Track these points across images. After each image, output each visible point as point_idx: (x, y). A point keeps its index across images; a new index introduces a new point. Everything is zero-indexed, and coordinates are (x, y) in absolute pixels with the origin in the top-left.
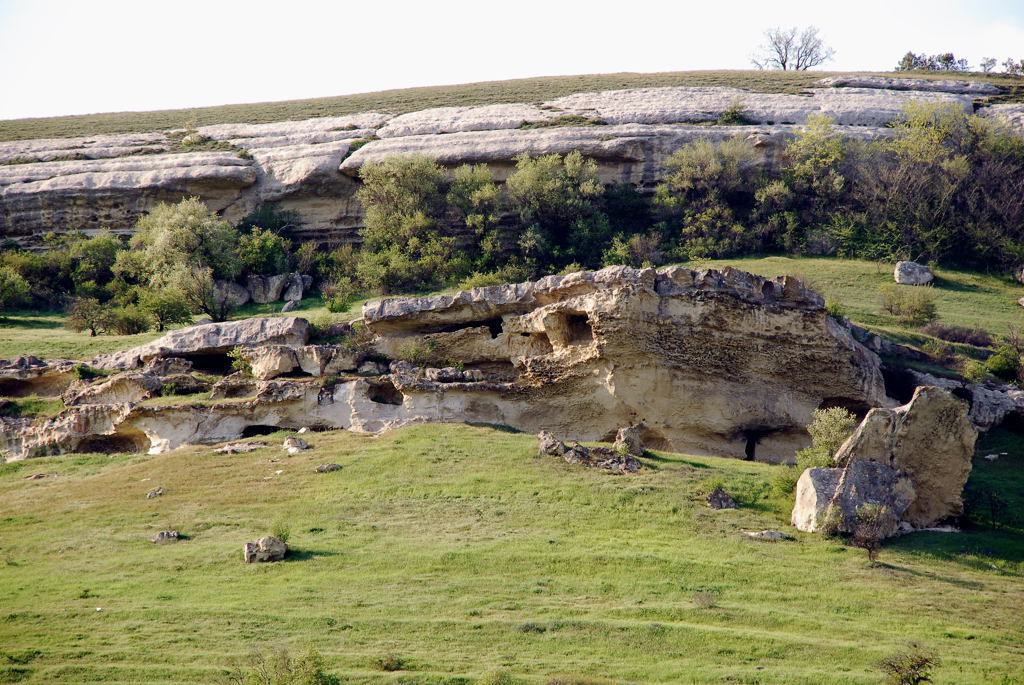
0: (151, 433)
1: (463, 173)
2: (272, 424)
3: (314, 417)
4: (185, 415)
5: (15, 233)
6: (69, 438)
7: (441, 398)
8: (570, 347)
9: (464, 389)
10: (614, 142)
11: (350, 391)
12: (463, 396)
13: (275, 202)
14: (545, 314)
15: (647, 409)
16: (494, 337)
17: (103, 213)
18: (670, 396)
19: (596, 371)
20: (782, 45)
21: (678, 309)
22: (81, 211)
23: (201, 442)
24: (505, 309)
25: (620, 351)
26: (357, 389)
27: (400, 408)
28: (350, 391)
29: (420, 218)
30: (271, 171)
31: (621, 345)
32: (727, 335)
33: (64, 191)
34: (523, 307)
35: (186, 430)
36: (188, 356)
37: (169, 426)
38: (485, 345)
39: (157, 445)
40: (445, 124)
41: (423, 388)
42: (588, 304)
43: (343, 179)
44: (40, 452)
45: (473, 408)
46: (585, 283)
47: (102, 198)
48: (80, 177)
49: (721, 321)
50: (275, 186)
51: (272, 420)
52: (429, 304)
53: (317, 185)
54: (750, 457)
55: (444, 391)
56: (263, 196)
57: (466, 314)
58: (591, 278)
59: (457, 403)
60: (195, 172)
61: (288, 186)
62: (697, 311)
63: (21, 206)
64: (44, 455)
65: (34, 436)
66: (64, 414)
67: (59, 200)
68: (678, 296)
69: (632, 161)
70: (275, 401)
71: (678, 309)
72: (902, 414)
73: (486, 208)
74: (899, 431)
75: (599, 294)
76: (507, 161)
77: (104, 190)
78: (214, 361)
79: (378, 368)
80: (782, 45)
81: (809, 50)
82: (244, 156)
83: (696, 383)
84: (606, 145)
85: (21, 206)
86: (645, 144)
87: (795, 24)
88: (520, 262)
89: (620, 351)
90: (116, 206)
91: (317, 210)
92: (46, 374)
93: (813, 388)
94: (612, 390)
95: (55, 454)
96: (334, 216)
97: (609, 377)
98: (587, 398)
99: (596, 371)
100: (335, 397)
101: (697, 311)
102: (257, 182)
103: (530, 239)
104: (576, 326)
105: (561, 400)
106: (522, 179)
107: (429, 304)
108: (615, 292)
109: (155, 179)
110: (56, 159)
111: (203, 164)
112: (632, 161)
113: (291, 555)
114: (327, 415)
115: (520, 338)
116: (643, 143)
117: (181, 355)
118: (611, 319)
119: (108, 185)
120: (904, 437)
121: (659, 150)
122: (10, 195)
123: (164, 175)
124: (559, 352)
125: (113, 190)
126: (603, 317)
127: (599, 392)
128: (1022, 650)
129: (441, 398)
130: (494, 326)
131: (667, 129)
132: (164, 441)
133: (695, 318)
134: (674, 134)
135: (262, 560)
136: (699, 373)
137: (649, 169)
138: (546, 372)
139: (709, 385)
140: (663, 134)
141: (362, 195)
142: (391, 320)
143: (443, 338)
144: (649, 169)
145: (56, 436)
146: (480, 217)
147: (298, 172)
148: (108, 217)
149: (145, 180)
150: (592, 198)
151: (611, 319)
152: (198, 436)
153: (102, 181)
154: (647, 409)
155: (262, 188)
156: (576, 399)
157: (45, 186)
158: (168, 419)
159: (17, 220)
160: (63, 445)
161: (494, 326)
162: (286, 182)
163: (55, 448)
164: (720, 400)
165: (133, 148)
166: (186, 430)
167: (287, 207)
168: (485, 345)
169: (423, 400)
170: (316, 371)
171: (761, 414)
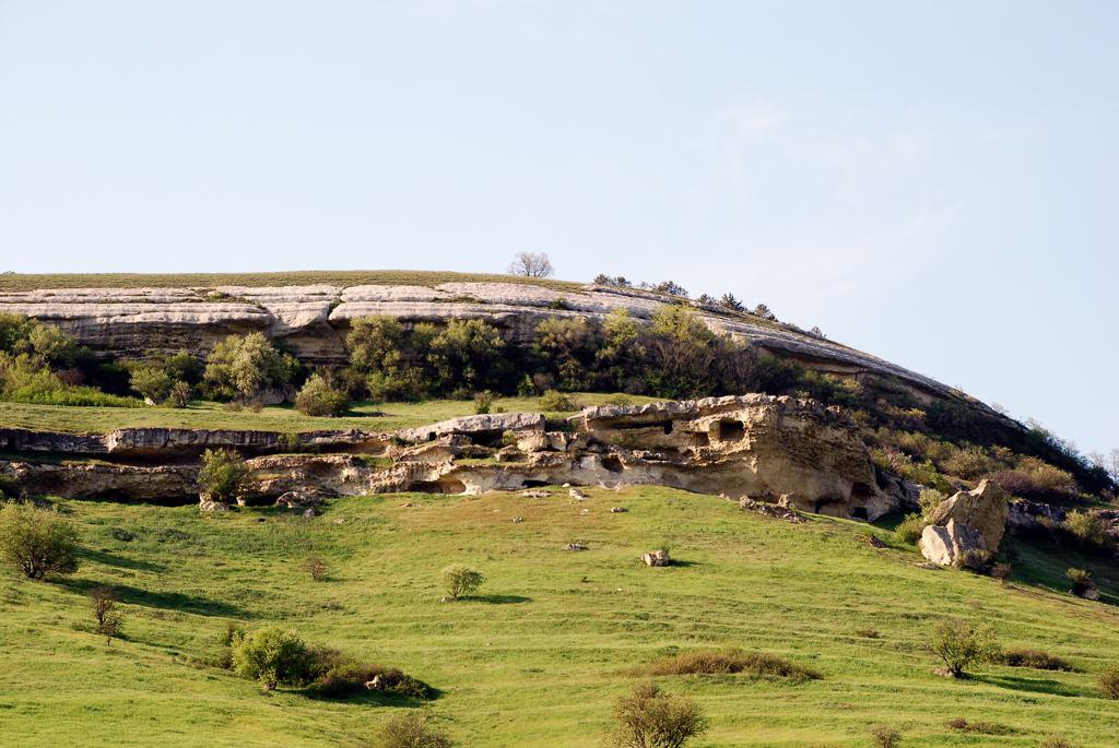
0: (468, 482)
1: (419, 327)
2: (543, 480)
3: (569, 476)
4: (490, 471)
5: (113, 348)
6: (404, 482)
7: (648, 470)
8: (725, 443)
9: (661, 465)
10: (501, 315)
11: (591, 461)
12: (661, 469)
13: (284, 337)
14: (711, 421)
15: (774, 484)
16: (667, 434)
17: (173, 339)
18: (789, 476)
19: (745, 458)
20: (527, 262)
21: (789, 422)
22: (160, 336)
23: (501, 489)
24: (678, 416)
25: (762, 447)
26: (596, 461)
27: (623, 474)
28: (591, 461)
29: (396, 355)
30: (280, 318)
31: (764, 443)
32: (815, 441)
33: (153, 323)
34: (692, 415)
35: (491, 481)
36: (469, 434)
37: (480, 478)
38: (662, 438)
39: (471, 489)
40: (385, 296)
41: (637, 463)
42: (743, 416)
43: (329, 327)
44: (383, 490)
45: (663, 477)
46: (736, 404)
47: (175, 329)
48: (161, 315)
49: (813, 432)
50: (284, 328)
51: (543, 477)
52: (628, 411)
53: (313, 330)
54: (817, 513)
55: (650, 465)
56: (274, 334)
57: (650, 418)
58: (740, 400)
59: (657, 473)
60: (236, 316)
61: (293, 328)
62: (802, 425)
63: (122, 331)
64: (385, 491)
65: (380, 480)
66: (397, 467)
67: (147, 328)
68: (788, 415)
69: (508, 327)
70: (547, 466)
71: (789, 422)
72: (977, 495)
73: (439, 351)
74: (974, 506)
75: (751, 411)
76: (440, 322)
77: (177, 324)
78: (489, 438)
79: (992, 455)
80: (527, 262)
81: (545, 267)
82: (260, 307)
83: (801, 469)
84: (496, 316)
85: (122, 331)
86: (516, 318)
87: (535, 250)
88: (465, 386)
89: (762, 447)
90: (182, 334)
91: (307, 345)
92: (369, 441)
93: (850, 476)
94: (755, 470)
95: (392, 492)
96: (317, 349)
97: (753, 463)
98: (734, 475)
99: (745, 458)
100: (582, 465)
101: (802, 425)
102: (271, 325)
103: (470, 373)
104: (730, 429)
105: (717, 475)
106: (456, 333)
107: (628, 411)
108: (761, 410)
109: (211, 319)
110: (132, 302)
111: (238, 311)
112: (508, 327)
113: (672, 563)
114: (578, 477)
115: (685, 435)
116: (516, 317)
117: (466, 433)
118: (760, 426)
119: (180, 320)
120: (976, 510)
121: (524, 322)
122: (115, 323)
123: (216, 317)
124: (715, 445)
125: (183, 324)
126: (756, 425)
127: (745, 471)
128: (1117, 629)
129: (648, 470)
130: (667, 426)
131: (528, 309)
132: (477, 487)
133: (801, 429)
134: (533, 313)
135: (658, 565)
136: (803, 464)
137: (517, 334)
138: (706, 456)
139: (808, 471)
140: (526, 312)
141: (350, 338)
142: (604, 419)
143: (634, 431)
144: (517, 334)
145: (396, 481)
146: (437, 357)
147: (302, 319)
148: (175, 341)
149: (203, 319)
150: (499, 348)
151: (760, 426)
152: (499, 485)
153: (176, 318)
154: (774, 484)
155: (274, 328)
156: (727, 475)
157: (138, 319)
158: (480, 474)
159: (117, 340)
160: (400, 486)
161: (667, 426)
162: (291, 326)
163: (393, 488)
164: (813, 480)
165: (181, 298)
166: (491, 481)
167: (290, 342)
168: (662, 438)
169: (637, 471)
170: (563, 448)
171: (831, 490)
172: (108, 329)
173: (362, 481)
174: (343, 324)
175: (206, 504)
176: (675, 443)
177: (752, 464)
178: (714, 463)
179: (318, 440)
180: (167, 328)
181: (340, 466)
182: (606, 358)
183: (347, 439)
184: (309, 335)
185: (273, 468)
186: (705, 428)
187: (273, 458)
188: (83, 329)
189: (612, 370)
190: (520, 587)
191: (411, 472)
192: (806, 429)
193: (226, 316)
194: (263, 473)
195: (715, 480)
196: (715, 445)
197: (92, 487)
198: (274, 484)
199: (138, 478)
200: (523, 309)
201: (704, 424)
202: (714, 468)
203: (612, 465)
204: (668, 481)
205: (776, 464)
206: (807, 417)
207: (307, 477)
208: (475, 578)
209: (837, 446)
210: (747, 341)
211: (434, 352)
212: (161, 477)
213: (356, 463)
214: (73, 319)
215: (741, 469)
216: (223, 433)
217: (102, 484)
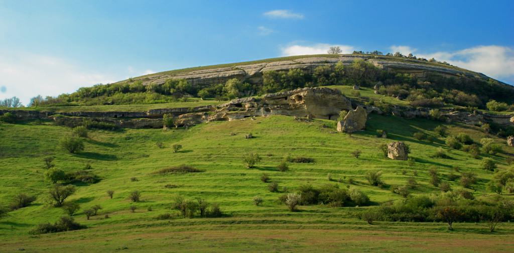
1: (280, 72)
3: (256, 114)
21: (317, 94)
34: (291, 94)
36: (235, 104)
38: (285, 101)
39: (230, 120)
40: (277, 64)
41: (274, 109)
42: (302, 94)
45: (283, 112)
51: (249, 115)
53: (256, 75)
54: (330, 119)
57: (281, 96)
59: (280, 111)
60: (235, 74)
62: (320, 95)
67: (213, 79)
71: (317, 94)
73: (284, 78)
76: (287, 70)
84: (304, 67)
86: (311, 67)
88: (290, 87)
104: (300, 98)
105: (297, 110)
113: (253, 137)
114: (258, 114)
124: (297, 102)
126: (304, 96)
130: (286, 98)
138: (294, 105)
139: (322, 107)
141: (263, 76)
142: (268, 97)
143: (277, 100)
149: (227, 75)
150: (302, 76)
156: (300, 110)
157: (211, 77)
161: (286, 98)
163: (213, 120)
172: (204, 80)
173: (207, 120)
174: (262, 73)
175: (165, 128)
176: (288, 103)
177: (305, 107)
178: (296, 108)
179: (200, 109)
180: (218, 78)
181: (202, 115)
182: (332, 76)
183: (206, 108)
184: (255, 77)
185: (185, 117)
186: (294, 98)
187: (186, 115)
188: (199, 80)
189: (333, 79)
190: (192, 149)
191: (218, 116)
192: (321, 96)
193: (233, 74)
194: (181, 119)
195: (298, 112)
196: (297, 102)
197: (141, 125)
198: (184, 121)
199: (153, 122)
200: (313, 64)
201: (293, 97)
202: (296, 108)
203: (268, 110)
204: (283, 113)
205: (312, 106)
206: (322, 93)
207: (193, 119)
208: (180, 146)
209: (334, 99)
210: (208, 91)
211: (282, 79)
212: (158, 122)
213: (206, 114)
214: (196, 78)
215: (303, 108)
216: (175, 109)
217: (144, 124)
